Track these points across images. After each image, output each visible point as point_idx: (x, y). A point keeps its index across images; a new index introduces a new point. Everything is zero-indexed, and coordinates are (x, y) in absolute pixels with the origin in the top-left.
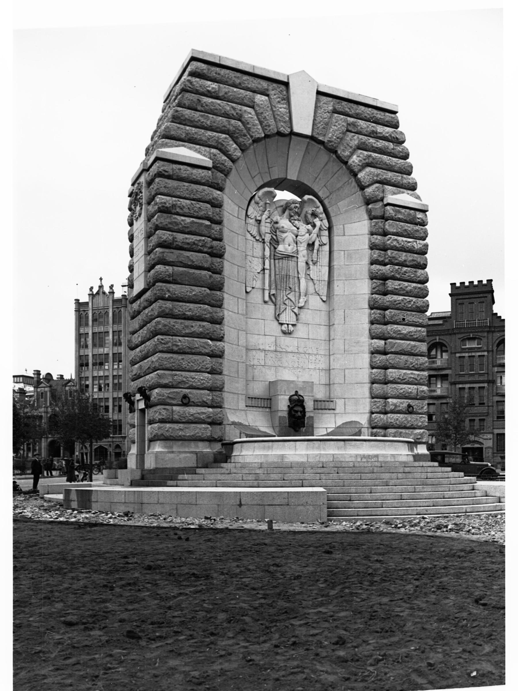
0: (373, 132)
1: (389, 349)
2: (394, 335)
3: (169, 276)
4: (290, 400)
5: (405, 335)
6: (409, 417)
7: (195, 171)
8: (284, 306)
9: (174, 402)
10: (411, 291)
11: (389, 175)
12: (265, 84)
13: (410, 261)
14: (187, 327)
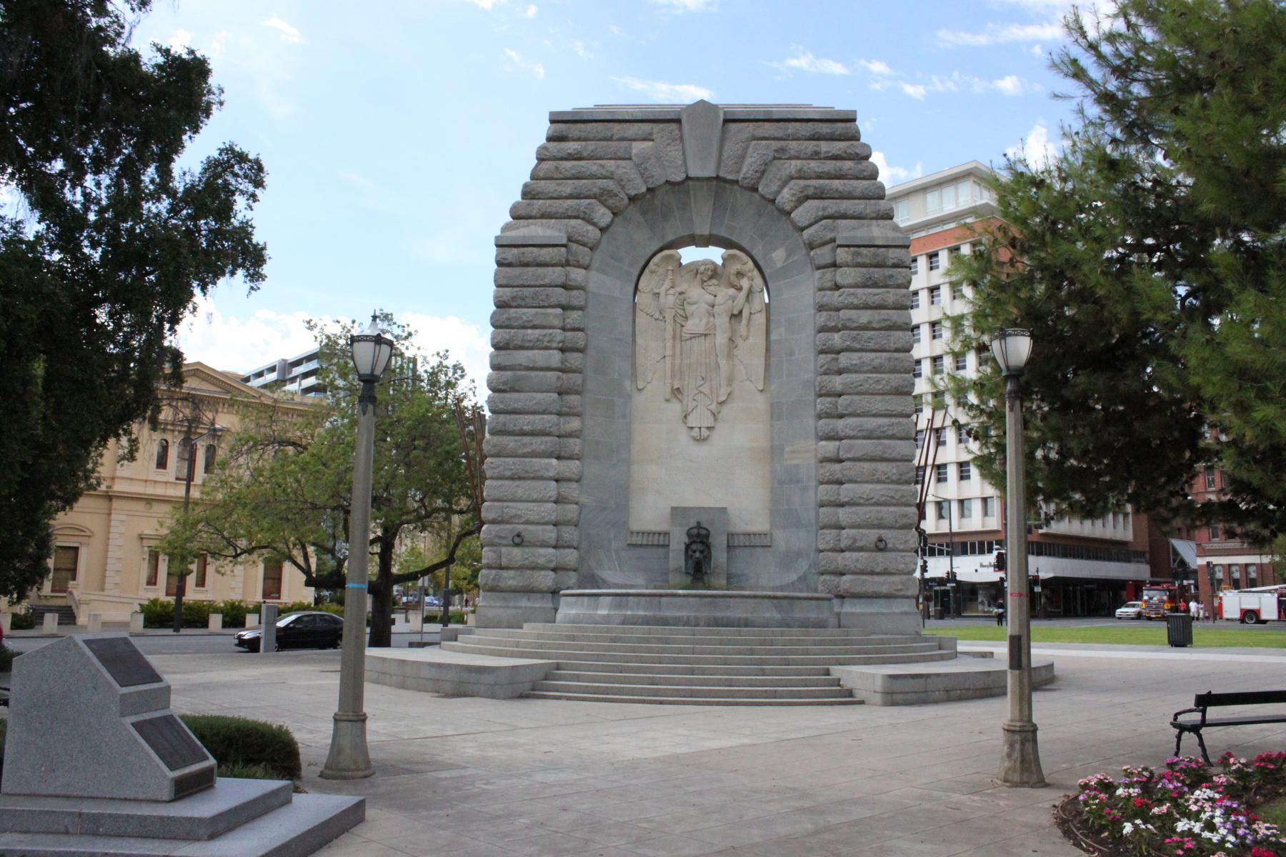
0: (817, 153)
1: (843, 455)
2: (852, 433)
3: (504, 383)
4: (689, 535)
5: (871, 432)
6: (880, 556)
7: (544, 251)
8: (694, 403)
9: (504, 542)
10: (881, 365)
11: (844, 205)
12: (646, 127)
13: (879, 322)
14: (525, 445)
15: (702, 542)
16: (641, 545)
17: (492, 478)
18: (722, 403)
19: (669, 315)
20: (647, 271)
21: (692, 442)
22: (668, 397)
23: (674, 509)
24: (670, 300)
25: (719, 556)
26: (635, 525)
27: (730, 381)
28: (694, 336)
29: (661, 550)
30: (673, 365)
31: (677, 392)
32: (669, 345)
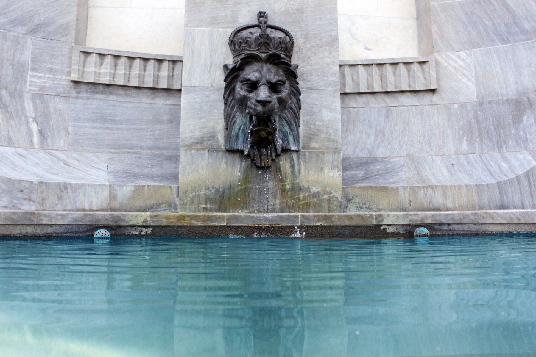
4: (236, 42)
15: (275, 60)
17: (339, 288)
25: (320, 108)
29: (162, 103)
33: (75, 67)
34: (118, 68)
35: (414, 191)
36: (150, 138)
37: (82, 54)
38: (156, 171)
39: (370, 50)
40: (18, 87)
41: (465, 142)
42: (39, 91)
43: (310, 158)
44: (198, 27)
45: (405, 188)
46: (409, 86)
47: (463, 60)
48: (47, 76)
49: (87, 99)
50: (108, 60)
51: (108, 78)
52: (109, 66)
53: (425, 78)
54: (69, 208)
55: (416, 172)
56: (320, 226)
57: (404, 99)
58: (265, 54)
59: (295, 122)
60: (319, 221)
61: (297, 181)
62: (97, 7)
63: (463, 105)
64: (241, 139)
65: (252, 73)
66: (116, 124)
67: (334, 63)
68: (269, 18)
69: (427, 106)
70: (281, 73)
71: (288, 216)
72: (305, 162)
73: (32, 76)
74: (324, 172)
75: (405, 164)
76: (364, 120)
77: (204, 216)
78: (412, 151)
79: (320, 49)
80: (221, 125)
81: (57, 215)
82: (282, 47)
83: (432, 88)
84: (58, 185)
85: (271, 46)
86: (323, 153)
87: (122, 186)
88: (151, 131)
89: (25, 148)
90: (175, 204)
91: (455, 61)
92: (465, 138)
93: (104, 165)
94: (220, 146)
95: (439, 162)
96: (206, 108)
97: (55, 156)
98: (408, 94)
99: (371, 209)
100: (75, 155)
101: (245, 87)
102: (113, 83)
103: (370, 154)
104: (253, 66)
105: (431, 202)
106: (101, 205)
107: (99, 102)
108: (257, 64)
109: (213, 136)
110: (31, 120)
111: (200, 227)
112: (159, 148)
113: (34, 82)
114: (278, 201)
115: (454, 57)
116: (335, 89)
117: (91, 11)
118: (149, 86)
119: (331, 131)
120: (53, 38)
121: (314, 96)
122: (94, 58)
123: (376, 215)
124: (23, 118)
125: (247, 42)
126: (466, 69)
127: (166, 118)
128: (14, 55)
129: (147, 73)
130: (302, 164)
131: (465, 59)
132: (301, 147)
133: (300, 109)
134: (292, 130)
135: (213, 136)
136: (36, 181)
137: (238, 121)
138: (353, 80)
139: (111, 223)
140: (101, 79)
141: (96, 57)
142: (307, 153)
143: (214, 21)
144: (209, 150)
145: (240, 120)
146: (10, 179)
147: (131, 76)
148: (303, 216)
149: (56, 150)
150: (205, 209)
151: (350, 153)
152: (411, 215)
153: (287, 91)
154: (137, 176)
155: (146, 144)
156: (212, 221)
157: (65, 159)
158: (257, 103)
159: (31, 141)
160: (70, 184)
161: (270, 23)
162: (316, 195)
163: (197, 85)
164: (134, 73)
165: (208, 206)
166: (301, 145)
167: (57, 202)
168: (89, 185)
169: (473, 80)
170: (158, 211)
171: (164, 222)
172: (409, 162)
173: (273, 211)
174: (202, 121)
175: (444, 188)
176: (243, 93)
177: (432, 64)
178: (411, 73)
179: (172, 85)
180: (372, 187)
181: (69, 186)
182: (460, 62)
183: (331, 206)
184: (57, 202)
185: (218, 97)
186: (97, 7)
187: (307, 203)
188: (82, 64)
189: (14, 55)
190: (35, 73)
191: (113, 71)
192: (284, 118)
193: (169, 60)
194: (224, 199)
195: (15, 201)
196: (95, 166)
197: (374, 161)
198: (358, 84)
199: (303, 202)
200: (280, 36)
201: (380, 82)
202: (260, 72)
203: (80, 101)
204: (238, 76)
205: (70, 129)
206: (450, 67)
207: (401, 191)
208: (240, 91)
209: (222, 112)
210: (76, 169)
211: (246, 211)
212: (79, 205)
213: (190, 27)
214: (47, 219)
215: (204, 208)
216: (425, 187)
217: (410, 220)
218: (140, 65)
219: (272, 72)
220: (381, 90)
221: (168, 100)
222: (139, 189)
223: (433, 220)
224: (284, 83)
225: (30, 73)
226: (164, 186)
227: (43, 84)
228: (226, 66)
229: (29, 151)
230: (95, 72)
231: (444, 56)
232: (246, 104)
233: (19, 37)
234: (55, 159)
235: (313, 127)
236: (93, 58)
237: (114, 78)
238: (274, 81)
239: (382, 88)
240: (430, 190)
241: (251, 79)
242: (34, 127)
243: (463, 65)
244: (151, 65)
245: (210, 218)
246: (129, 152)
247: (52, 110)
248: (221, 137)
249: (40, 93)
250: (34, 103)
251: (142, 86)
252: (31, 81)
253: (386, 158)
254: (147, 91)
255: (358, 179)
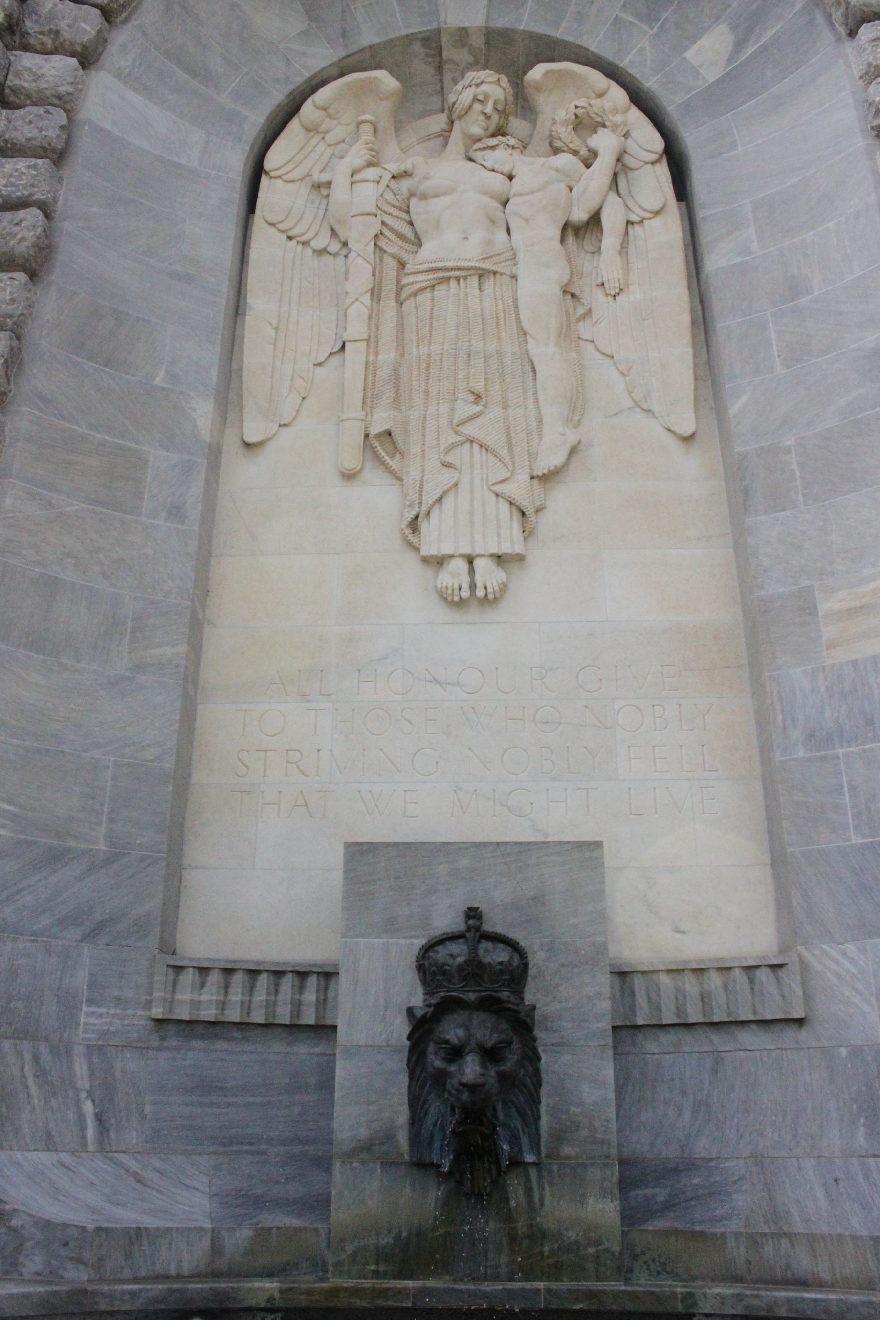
4: (428, 967)
8: (448, 477)
15: (489, 1005)
16: (215, 1028)
18: (547, 478)
19: (360, 234)
20: (294, 125)
21: (442, 613)
22: (351, 462)
23: (359, 853)
24: (361, 198)
25: (580, 1077)
26: (205, 937)
27: (576, 407)
28: (445, 276)
29: (305, 1051)
30: (370, 369)
31: (381, 446)
32: (359, 310)
33: (158, 994)
34: (231, 990)
35: (755, 1242)
36: (285, 1122)
37: (170, 971)
38: (295, 1190)
39: (684, 932)
40: (66, 1035)
41: (862, 1129)
42: (99, 1039)
43: (559, 1175)
44: (363, 936)
45: (737, 1235)
46: (755, 1012)
47: (852, 960)
48: (112, 1012)
49: (178, 1049)
50: (215, 978)
51: (213, 1012)
52: (214, 989)
53: (783, 997)
54: (143, 1273)
55: (765, 1194)
56: (581, 1311)
57: (748, 1038)
58: (476, 995)
59: (532, 1111)
60: (577, 1300)
61: (538, 1220)
62: (196, 867)
63: (856, 1051)
64: (437, 1145)
65: (453, 1031)
66: (225, 1096)
67: (601, 995)
68: (484, 917)
69: (788, 1052)
70: (504, 1025)
71: (523, 1290)
72: (551, 1183)
73: (88, 1015)
74: (587, 1203)
75: (748, 1176)
76: (673, 1080)
77: (373, 1289)
78: (761, 1146)
79: (576, 971)
80: (402, 1117)
81: (123, 1292)
82: (504, 980)
83: (796, 1016)
84: (127, 1231)
85: (486, 978)
86: (584, 1166)
87: (231, 1230)
88: (287, 1107)
89: (73, 1153)
90: (323, 1262)
91: (837, 962)
92: (862, 1121)
93: (204, 1180)
94: (402, 1155)
95: (811, 1173)
96: (377, 1086)
97: (122, 1166)
98: (754, 1027)
99: (677, 1275)
100: (156, 1163)
101: (442, 1054)
102: (222, 1019)
103: (683, 1151)
104: (455, 1016)
105: (788, 1266)
106: (197, 1266)
107: (197, 1055)
108: (462, 1012)
109: (389, 1137)
110: (83, 1095)
111: (365, 1310)
112: (301, 1142)
113: (91, 1024)
114: (504, 1259)
115: (835, 954)
116: (602, 1043)
117: (187, 875)
118: (283, 1022)
119: (597, 1124)
120: (124, 943)
121: (566, 1058)
122: (190, 977)
123: (682, 1293)
124: (71, 1093)
125: (444, 973)
126: (857, 978)
127: (312, 1081)
128: (60, 980)
129: (280, 997)
130: (547, 1188)
131: (856, 958)
132: (543, 1155)
133: (540, 1085)
134: (526, 1125)
135: (389, 1137)
136: (91, 1227)
137: (432, 1111)
138: (649, 998)
139: (211, 1305)
140: (202, 1013)
141: (194, 974)
142: (555, 1167)
143: (391, 927)
144: (382, 1163)
145: (435, 1107)
146: (48, 1222)
147: (254, 1005)
148: (549, 1291)
149: (124, 1152)
150: (376, 1274)
151: (646, 1148)
152: (746, 1296)
153: (515, 1057)
154: (259, 1203)
155: (277, 1133)
156: (387, 1300)
157: (139, 1171)
158: (461, 1088)
159: (84, 1137)
160: (146, 1228)
161: (487, 927)
162: (574, 1247)
163: (362, 1043)
164: (258, 998)
165: (382, 1268)
166: (544, 1151)
167: (123, 1264)
168: (177, 1229)
169: (873, 1000)
170: (294, 1276)
171: (303, 1301)
172: (754, 1170)
173: (496, 1278)
174: (371, 1108)
175: (812, 1239)
176: (438, 1064)
177: (795, 967)
178: (756, 987)
179: (324, 1017)
180: (677, 1232)
181: (144, 1234)
182: (848, 965)
183: (602, 1269)
184: (123, 1264)
185: (399, 1063)
186: (196, 867)
187: (557, 1262)
188: (171, 988)
189: (60, 980)
190: (93, 1009)
191: (222, 998)
192: (513, 1104)
193: (318, 973)
194: (411, 1253)
195: (54, 1262)
196: (187, 1182)
197: (689, 1165)
198: (659, 1008)
199: (551, 1261)
200: (500, 959)
201: (700, 1004)
202: (467, 1029)
203: (165, 1054)
204: (430, 1031)
205: (148, 1109)
206: (829, 975)
207: (731, 1242)
208: (436, 1062)
209: (405, 1091)
210: (158, 1191)
211: (447, 1278)
212: (159, 1268)
213: (351, 937)
214: (107, 1300)
215: (373, 1271)
216: (777, 1236)
217: (746, 1308)
218: (268, 984)
219: (487, 1028)
220: (701, 1020)
221: (317, 1045)
222: (262, 1234)
223: (789, 1310)
224: (510, 1043)
225: (85, 1009)
226: (305, 1228)
227: (106, 1028)
228: (410, 1011)
229: (79, 1157)
230: (192, 1001)
231: (817, 952)
232: (444, 1084)
233: (69, 946)
234: (122, 1172)
235: (564, 1116)
236: (188, 977)
237: (223, 1009)
238: (490, 1044)
239: (704, 1016)
240: (785, 1242)
241: (452, 1041)
242: (88, 1107)
243: (853, 970)
244: (287, 984)
245: (383, 1293)
246: (247, 1152)
247: (118, 1074)
248: (403, 1138)
249: (100, 1043)
250: (89, 1061)
251: (271, 1021)
252: (85, 1024)
253: (712, 1159)
254: (280, 1030)
255: (655, 1207)
